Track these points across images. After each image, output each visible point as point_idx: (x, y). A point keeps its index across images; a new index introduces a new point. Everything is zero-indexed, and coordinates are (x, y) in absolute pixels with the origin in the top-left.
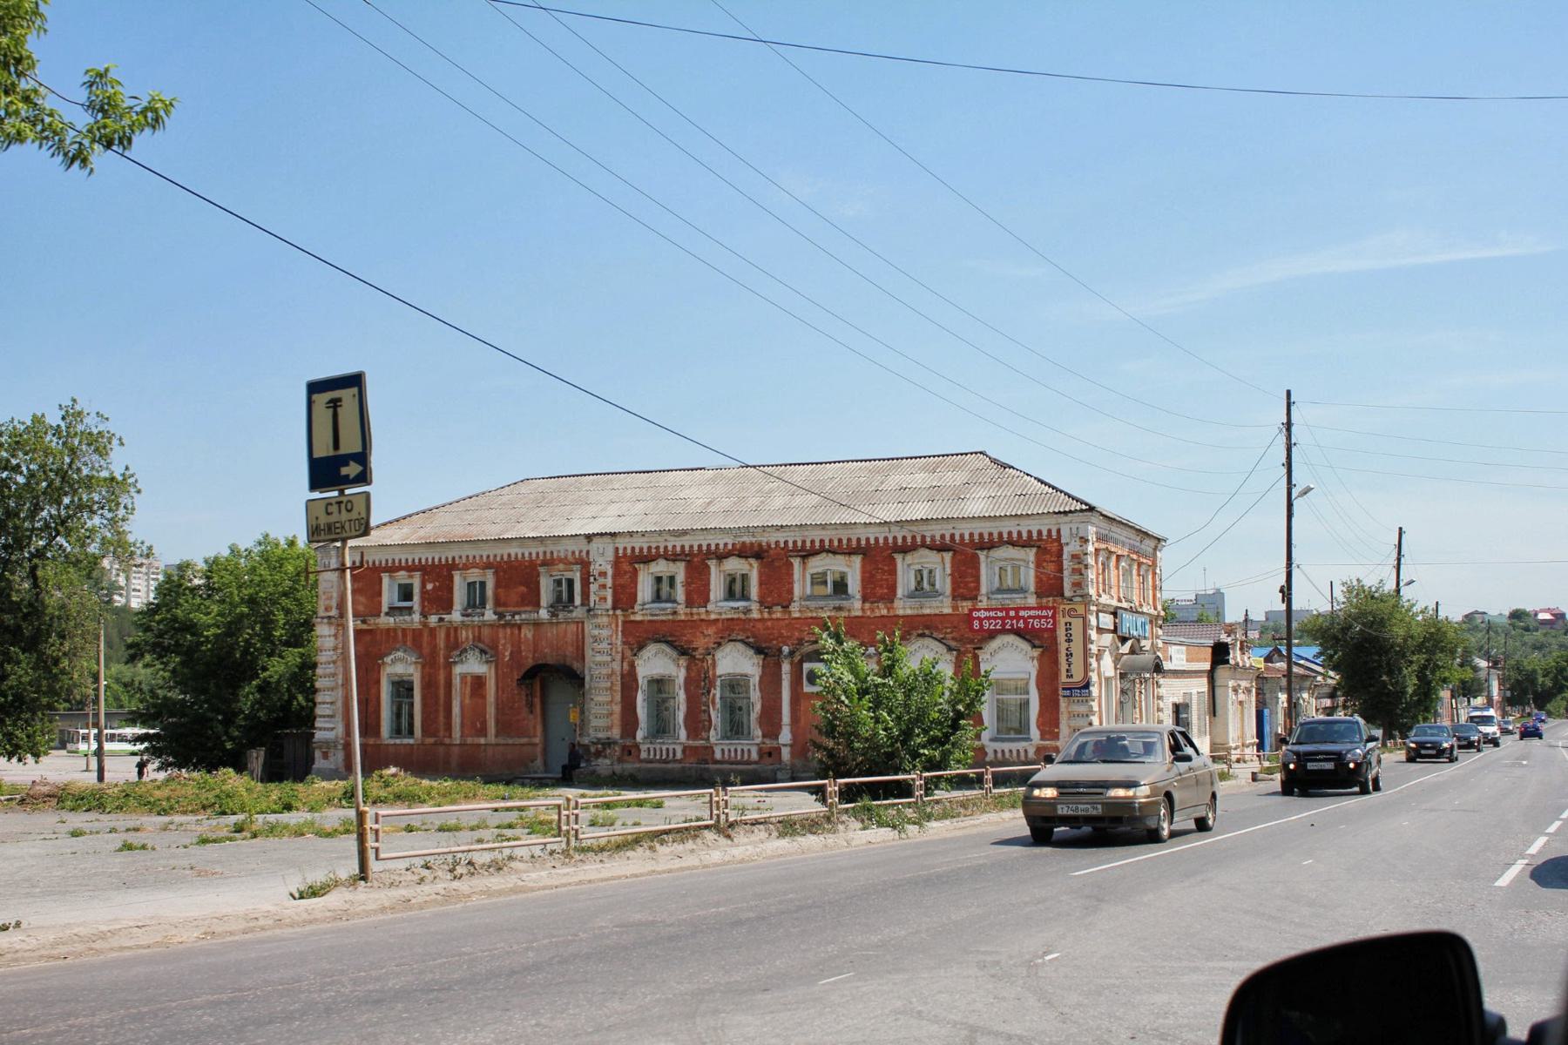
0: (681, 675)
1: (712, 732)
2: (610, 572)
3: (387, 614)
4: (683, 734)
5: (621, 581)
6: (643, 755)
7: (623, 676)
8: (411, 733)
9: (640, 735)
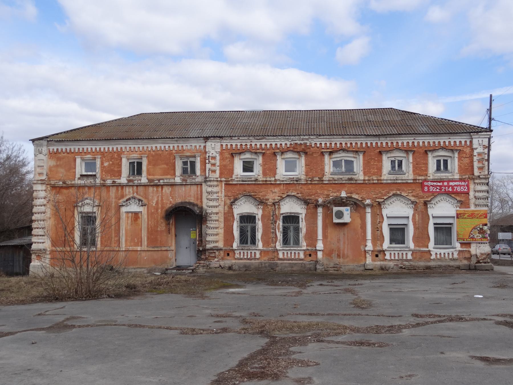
1: (278, 243)
3: (79, 179)
5: (224, 163)
6: (237, 256)
7: (225, 213)
9: (235, 245)
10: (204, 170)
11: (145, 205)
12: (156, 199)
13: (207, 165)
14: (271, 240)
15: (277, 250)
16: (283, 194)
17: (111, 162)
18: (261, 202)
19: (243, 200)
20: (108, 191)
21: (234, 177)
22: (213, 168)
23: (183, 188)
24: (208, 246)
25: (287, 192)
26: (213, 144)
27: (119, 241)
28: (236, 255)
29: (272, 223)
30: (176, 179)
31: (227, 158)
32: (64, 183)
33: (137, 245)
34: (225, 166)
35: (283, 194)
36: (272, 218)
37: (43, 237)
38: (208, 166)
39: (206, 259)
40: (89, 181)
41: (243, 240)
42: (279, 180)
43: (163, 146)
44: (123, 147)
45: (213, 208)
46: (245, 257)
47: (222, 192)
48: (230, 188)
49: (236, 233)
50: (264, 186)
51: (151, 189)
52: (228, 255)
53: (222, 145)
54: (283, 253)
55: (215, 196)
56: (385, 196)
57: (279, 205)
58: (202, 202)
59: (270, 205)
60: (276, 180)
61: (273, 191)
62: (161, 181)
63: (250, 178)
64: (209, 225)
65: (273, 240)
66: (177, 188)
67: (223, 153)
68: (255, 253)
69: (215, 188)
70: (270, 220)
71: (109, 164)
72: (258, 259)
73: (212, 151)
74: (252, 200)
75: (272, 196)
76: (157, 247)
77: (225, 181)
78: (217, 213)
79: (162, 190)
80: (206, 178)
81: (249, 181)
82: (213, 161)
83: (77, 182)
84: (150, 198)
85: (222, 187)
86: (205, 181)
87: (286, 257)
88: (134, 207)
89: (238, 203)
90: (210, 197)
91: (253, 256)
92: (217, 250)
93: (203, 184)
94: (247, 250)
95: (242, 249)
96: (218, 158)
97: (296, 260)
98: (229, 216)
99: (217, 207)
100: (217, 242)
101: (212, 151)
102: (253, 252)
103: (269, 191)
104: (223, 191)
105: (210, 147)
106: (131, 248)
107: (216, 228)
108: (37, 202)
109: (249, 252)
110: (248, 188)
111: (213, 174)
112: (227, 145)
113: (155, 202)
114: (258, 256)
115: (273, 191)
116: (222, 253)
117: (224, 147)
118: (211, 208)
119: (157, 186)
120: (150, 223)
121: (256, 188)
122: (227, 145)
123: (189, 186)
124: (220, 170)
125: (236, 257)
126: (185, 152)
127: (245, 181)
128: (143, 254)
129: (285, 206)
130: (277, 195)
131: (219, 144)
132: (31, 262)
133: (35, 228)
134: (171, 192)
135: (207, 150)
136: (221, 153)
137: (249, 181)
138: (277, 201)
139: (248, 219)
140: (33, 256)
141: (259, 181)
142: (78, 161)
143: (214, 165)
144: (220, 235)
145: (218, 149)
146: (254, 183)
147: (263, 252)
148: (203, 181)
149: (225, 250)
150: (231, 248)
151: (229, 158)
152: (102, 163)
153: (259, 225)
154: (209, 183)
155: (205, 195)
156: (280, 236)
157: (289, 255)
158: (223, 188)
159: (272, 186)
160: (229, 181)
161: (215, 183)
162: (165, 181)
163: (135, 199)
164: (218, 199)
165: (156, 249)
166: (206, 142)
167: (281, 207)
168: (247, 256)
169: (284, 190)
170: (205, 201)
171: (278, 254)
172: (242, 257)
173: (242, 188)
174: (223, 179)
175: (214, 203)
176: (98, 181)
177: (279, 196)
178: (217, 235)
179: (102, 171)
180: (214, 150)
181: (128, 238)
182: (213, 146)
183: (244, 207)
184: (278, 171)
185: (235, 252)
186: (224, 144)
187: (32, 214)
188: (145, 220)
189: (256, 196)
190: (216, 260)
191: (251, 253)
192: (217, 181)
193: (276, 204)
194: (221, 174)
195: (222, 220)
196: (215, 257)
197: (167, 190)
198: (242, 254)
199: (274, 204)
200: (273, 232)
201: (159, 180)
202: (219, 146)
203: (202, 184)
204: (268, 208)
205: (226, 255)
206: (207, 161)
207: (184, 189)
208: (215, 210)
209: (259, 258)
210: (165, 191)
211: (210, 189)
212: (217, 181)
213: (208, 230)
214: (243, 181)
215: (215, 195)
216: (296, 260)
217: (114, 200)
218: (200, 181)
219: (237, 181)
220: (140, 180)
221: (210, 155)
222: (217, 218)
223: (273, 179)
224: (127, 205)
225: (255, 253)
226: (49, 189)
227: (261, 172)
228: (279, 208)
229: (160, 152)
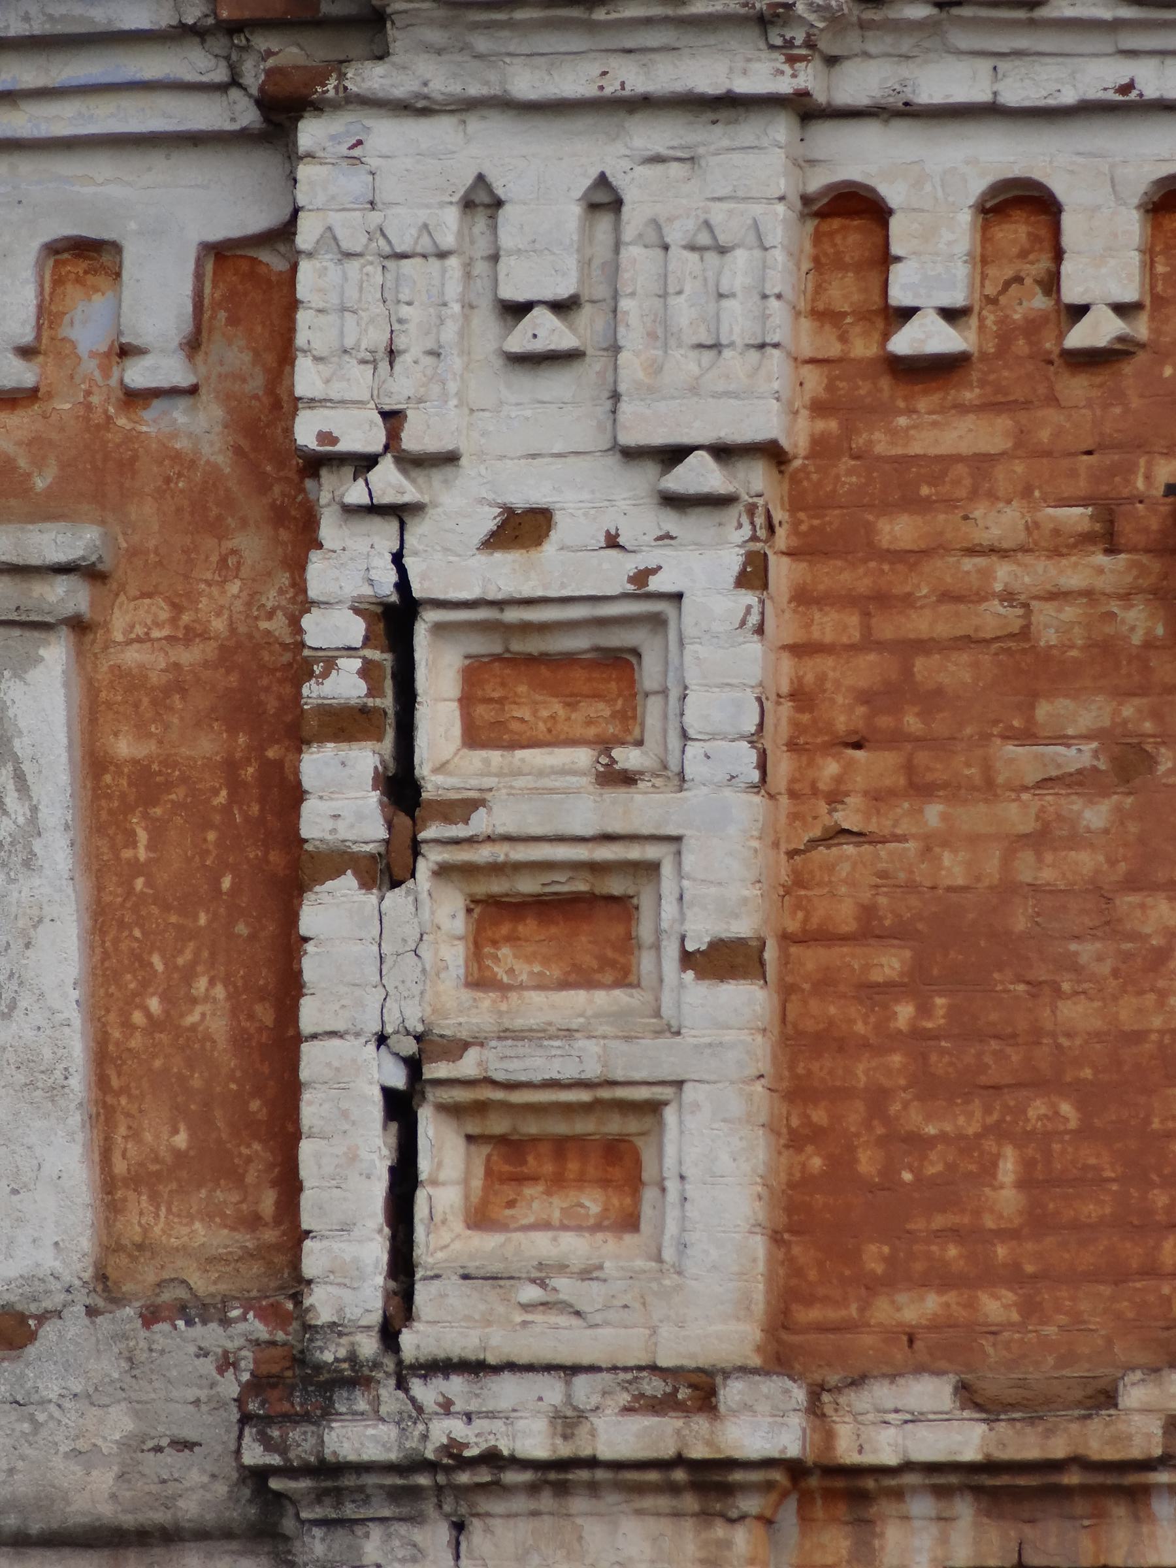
5: (949, 846)
13: (334, 914)
22: (556, 1031)
26: (543, 173)
31: (1027, 669)
34: (958, 945)
38: (376, 963)
39: (950, 503)
53: (852, 212)
67: (910, 483)
73: (516, 441)
80: (294, 1381)
82: (533, 795)
96: (722, 665)
101: (516, 441)
105: (434, 300)
111: (553, 1235)
112: (1023, 207)
117: (934, 263)
122: (1023, 207)
124: (807, 1078)
131: (760, 173)
135: (333, 406)
136: (826, 507)
143: (576, 911)
145: (725, 346)
166: (280, 116)
174: (910, 1421)
180: (560, 411)
182: (543, 250)
186: (933, 190)
194: (822, 1228)
202: (763, 267)
206: (340, 794)
221: (452, 563)
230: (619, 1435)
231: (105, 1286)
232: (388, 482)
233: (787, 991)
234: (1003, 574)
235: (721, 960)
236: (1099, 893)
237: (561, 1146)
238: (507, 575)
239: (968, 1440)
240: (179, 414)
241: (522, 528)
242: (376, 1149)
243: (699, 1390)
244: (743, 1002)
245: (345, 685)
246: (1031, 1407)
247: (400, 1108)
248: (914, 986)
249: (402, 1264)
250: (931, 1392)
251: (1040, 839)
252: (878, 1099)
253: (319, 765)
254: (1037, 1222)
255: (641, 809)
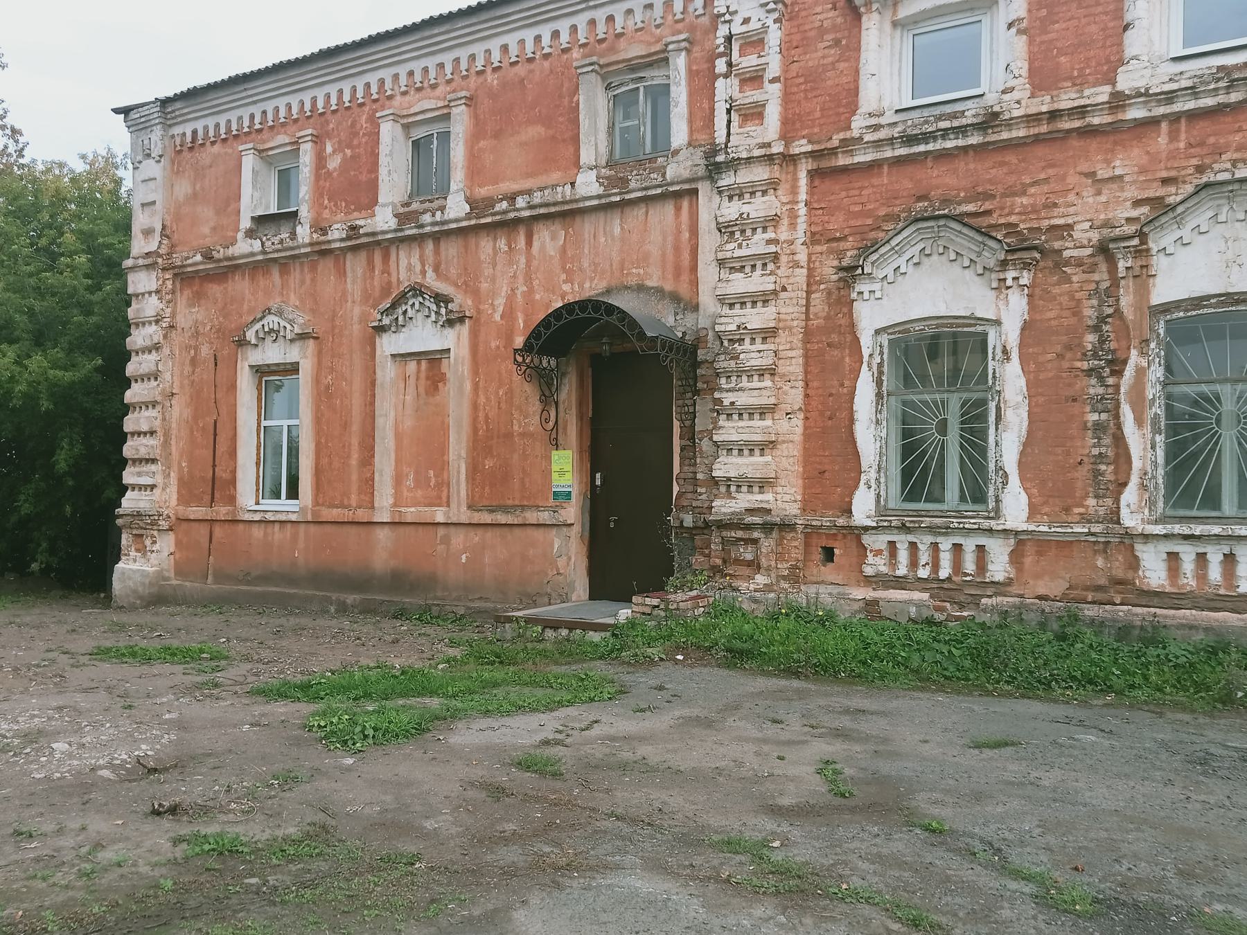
0: (1009, 314)
1: (1130, 496)
2: (774, 37)
3: (250, 234)
4: (1015, 507)
5: (813, 59)
6: (876, 564)
7: (808, 335)
8: (293, 493)
9: (863, 507)
10: (702, 118)
11: (461, 320)
12: (505, 290)
13: (720, 83)
14: (1084, 472)
15: (1129, 539)
16: (1165, 181)
17: (348, 152)
18: (1028, 253)
19: (911, 242)
20: (342, 273)
21: (858, 123)
22: (753, 96)
23: (615, 225)
24: (724, 507)
25: (1200, 169)
27: (368, 485)
28: (870, 558)
29: (1089, 372)
30: (580, 179)
31: (822, 31)
32: (208, 257)
33: (435, 502)
34: (813, 78)
35: (1165, 181)
36: (1091, 339)
37: (153, 467)
38: (724, 89)
40: (277, 239)
41: (918, 475)
42: (1145, 95)
43: (529, 35)
44: (386, 74)
45: (748, 310)
46: (923, 573)
47: (793, 216)
48: (837, 191)
49: (871, 437)
50: (1040, 151)
51: (486, 246)
52: (829, 554)
54: (1173, 557)
55: (757, 244)
56: (1034, 259)
57: (1142, 252)
58: (695, 283)
59: (1079, 263)
60: (1118, 101)
61: (1102, 173)
62: (521, 202)
63: (954, 116)
64: (727, 399)
65: (1097, 474)
66: (587, 226)
68: (981, 549)
69: (759, 199)
70: (1078, 359)
71: (344, 160)
72: (1000, 588)
74: (964, 241)
75: (1088, 209)
76: (505, 509)
77: (812, 154)
78: (768, 334)
79: (529, 243)
81: (945, 133)
82: (749, 62)
83: (245, 247)
84: (484, 286)
85: (794, 190)
86: (714, 170)
87: (1188, 579)
88: (422, 335)
89: (880, 267)
90: (732, 250)
91: (970, 566)
92: (768, 528)
93: (704, 188)
94: (932, 530)
95: (904, 528)
97: (1215, 602)
98: (829, 346)
99: (764, 298)
100: (764, 484)
102: (969, 544)
103: (1072, 179)
104: (802, 210)
106: (411, 513)
107: (763, 411)
108: (137, 339)
109: (946, 544)
110: (942, 179)
113: (500, 302)
114: (999, 568)
115: (1102, 173)
116: (795, 544)
118: (737, 310)
119: (508, 225)
120: (482, 400)
121: (988, 172)
123: (640, 211)
125: (869, 571)
126: (622, 43)
127: (926, 137)
128: (459, 539)
129: (1182, 253)
130: (1132, 193)
132: (118, 559)
133: (133, 434)
134: (563, 250)
137: (945, 133)
138: (1130, 229)
139: (941, 355)
140: (125, 539)
141: (1009, 124)
142: (249, 162)
144: (783, 449)
146: (974, 139)
147: (1030, 549)
148: (701, 171)
149: (811, 533)
150: (841, 522)
151: (835, 28)
152: (320, 160)
153: (1012, 381)
154: (726, 180)
155: (709, 241)
156: (1144, 447)
157: (1215, 573)
158: (803, 196)
159: (1093, 144)
160: (833, 152)
161: (760, 173)
162: (537, 198)
163: (422, 294)
164: (776, 257)
165: (502, 518)
167: (1160, 263)
168: (936, 566)
169: (1172, 156)
170: (708, 273)
171: (1134, 563)
172: (902, 571)
173: (905, 183)
175: (757, 282)
176: (304, 233)
177: (1137, 203)
178: (766, 446)
179: (318, 193)
181: (405, 469)
183: (920, 287)
184: (1134, 43)
185: (867, 539)
187: (127, 383)
188: (461, 388)
189: (983, 222)
190: (761, 579)
191: (957, 548)
192: (769, 158)
193: (1121, 251)
195: (794, 366)
196: (755, 565)
197: (548, 240)
198: (903, 556)
199: (1103, 250)
200: (1099, 427)
201: (512, 198)
203: (696, 191)
204: (1067, 279)
205: (818, 555)
206: (721, 66)
207: (617, 230)
208: (757, 318)
209: (1009, 582)
210: (543, 248)
211: (731, 210)
212: (769, 158)
213: (722, 421)
214: (910, 140)
215: (760, 236)
216: (1215, 602)
217: (357, 311)
218: (686, 174)
219: (878, 144)
220: (442, 209)
221: (737, 28)
222: (767, 361)
223: (1102, 94)
224: (398, 327)
225: (981, 549)
226: (169, 284)
227: (1021, 67)
228: (1143, 276)
229: (521, 70)
230: (757, 153)
231: (690, 144)
232: (727, 17)
233: (786, 87)
234: (819, 17)
235: (772, 81)
236: (833, 63)
237: (752, 114)
238: (744, 28)
239: (809, 148)
240: (703, 18)
241: (746, 21)
242: (725, 117)
243: (769, 145)
244: (777, 86)
245: (722, 49)
246: (819, 142)
247: (729, 111)
248: (806, 82)
249: (729, 134)
250: (804, 141)
251: (823, 57)
252: (799, 102)
253: (718, 62)
254: (823, 116)
255: (763, 60)
